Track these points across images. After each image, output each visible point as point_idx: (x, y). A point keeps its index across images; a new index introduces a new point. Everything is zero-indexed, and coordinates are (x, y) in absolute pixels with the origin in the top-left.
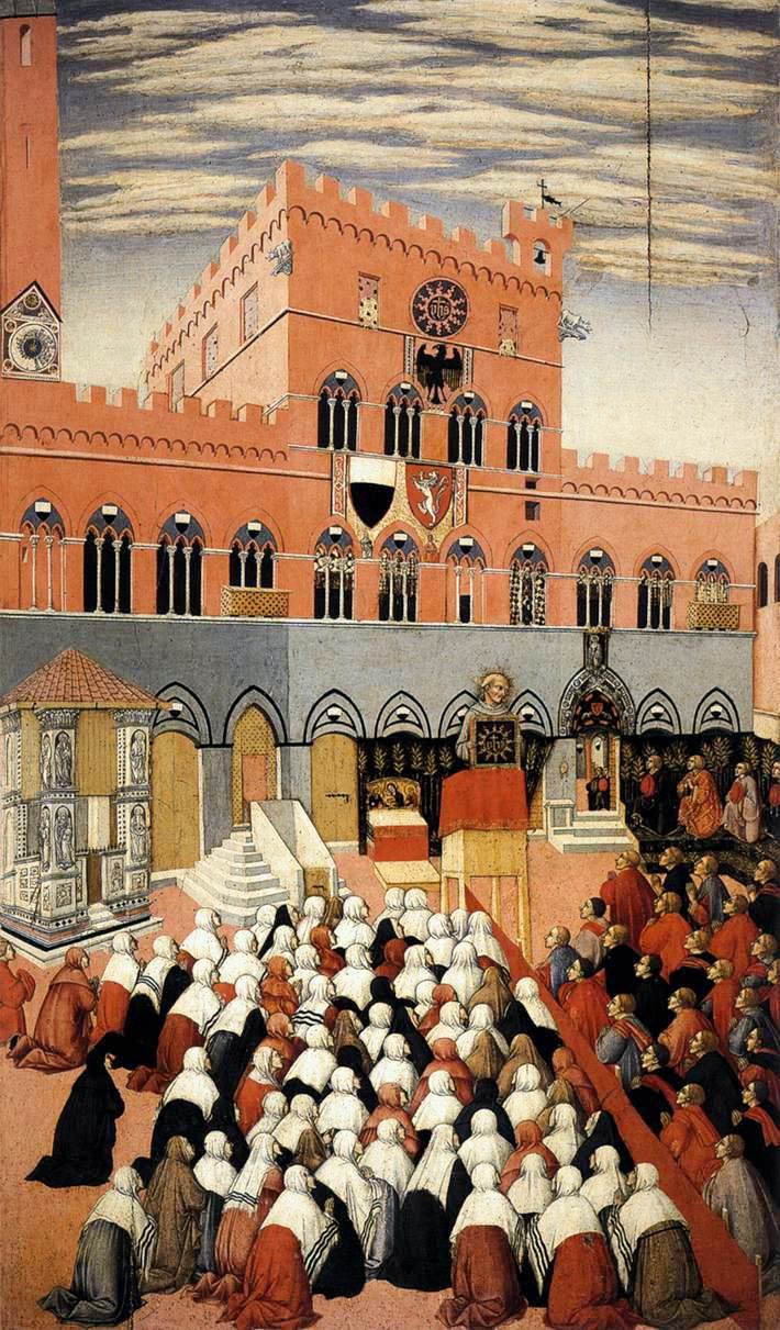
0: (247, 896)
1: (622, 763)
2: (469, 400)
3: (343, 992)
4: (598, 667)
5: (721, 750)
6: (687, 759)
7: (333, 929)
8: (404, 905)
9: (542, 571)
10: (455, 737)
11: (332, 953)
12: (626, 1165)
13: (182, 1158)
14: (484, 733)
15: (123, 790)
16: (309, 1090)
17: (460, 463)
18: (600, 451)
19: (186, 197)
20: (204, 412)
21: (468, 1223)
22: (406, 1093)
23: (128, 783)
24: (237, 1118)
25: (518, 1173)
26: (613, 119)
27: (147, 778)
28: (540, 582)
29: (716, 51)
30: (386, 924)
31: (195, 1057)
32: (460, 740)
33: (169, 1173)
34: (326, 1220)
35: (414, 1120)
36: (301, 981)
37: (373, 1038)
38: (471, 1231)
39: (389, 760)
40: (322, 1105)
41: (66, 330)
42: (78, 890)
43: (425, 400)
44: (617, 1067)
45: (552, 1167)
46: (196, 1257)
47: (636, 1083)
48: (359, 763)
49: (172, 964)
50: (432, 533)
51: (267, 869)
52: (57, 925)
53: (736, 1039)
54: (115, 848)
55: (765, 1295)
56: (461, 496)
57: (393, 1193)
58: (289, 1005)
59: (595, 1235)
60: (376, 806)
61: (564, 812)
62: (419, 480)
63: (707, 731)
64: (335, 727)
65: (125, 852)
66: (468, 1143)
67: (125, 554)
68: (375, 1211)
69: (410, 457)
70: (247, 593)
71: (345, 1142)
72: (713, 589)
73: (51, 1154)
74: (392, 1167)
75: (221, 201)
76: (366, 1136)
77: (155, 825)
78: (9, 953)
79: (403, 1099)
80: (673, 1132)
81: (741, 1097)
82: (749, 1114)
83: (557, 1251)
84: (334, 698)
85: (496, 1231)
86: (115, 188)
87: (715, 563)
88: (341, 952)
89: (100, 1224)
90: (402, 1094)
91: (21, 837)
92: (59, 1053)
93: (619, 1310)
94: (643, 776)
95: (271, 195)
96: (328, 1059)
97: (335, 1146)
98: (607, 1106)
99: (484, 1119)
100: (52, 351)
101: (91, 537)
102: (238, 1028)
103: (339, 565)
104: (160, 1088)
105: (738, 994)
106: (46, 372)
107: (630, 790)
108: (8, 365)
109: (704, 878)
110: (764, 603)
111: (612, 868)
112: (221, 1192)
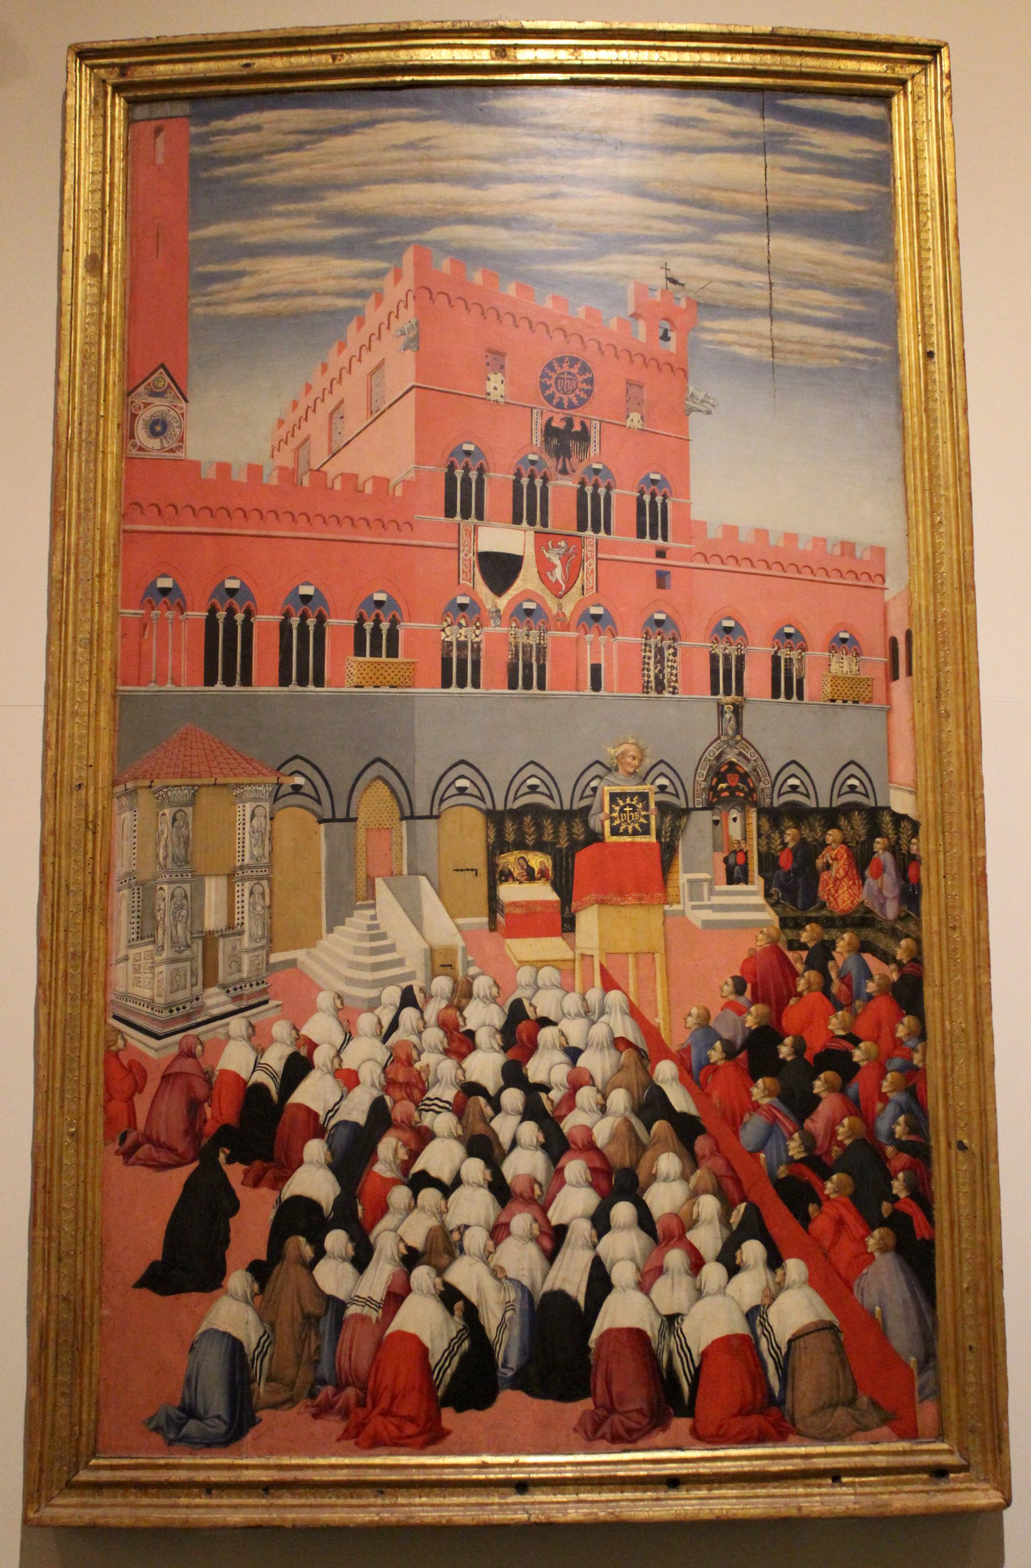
0: (369, 976)
1: (759, 836)
2: (597, 471)
3: (473, 1077)
4: (733, 738)
5: (859, 824)
6: (824, 833)
7: (461, 1009)
8: (536, 982)
9: (674, 640)
10: (588, 808)
11: (462, 1037)
12: (774, 1261)
13: (301, 1260)
14: (617, 804)
15: (241, 867)
16: (436, 1183)
17: (589, 533)
18: (730, 523)
19: (314, 280)
20: (329, 485)
21: (606, 1326)
22: (540, 1185)
23: (247, 861)
24: (360, 1214)
25: (660, 1271)
26: (734, 209)
27: (267, 854)
28: (671, 651)
29: (829, 152)
30: (518, 1005)
31: (315, 1149)
32: (592, 812)
33: (286, 1274)
34: (456, 1324)
35: (550, 1214)
36: (428, 1066)
37: (504, 1127)
38: (610, 1334)
39: (520, 832)
40: (451, 1199)
41: (193, 409)
42: (193, 973)
43: (553, 470)
44: (762, 1155)
45: (696, 1263)
46: (316, 1368)
47: (782, 1172)
48: (488, 836)
49: (289, 1051)
50: (561, 601)
51: (392, 948)
52: (171, 1011)
53: (882, 1125)
54: (232, 929)
55: (921, 1401)
56: (590, 565)
57: (527, 1293)
58: (416, 1093)
59: (742, 1337)
60: (506, 880)
61: (701, 887)
62: (547, 549)
63: (843, 805)
64: (462, 799)
65: (242, 933)
66: (606, 1239)
67: (248, 626)
68: (508, 1315)
69: (538, 527)
70: (372, 663)
71: (476, 1239)
72: (845, 662)
73: (160, 1258)
74: (526, 1265)
75: (349, 283)
76: (498, 1232)
77: (275, 903)
78: (120, 1043)
79: (537, 1191)
80: (821, 1221)
81: (890, 1187)
82: (899, 1205)
83: (704, 1354)
84: (462, 769)
85: (638, 1335)
86: (241, 274)
87: (846, 635)
88: (471, 1034)
89: (213, 1333)
90: (536, 1187)
91: (135, 920)
92: (171, 1149)
93: (772, 1419)
94: (781, 850)
95: (398, 277)
96: (458, 1150)
97: (466, 1243)
98: (753, 1197)
99: (623, 1211)
100: (178, 431)
101: (213, 611)
102: (360, 1117)
103: (466, 633)
104: (280, 1181)
105: (883, 1077)
106: (172, 451)
107: (768, 863)
108: (134, 445)
109: (846, 955)
110: (896, 677)
111: (752, 944)
112: (341, 1295)
